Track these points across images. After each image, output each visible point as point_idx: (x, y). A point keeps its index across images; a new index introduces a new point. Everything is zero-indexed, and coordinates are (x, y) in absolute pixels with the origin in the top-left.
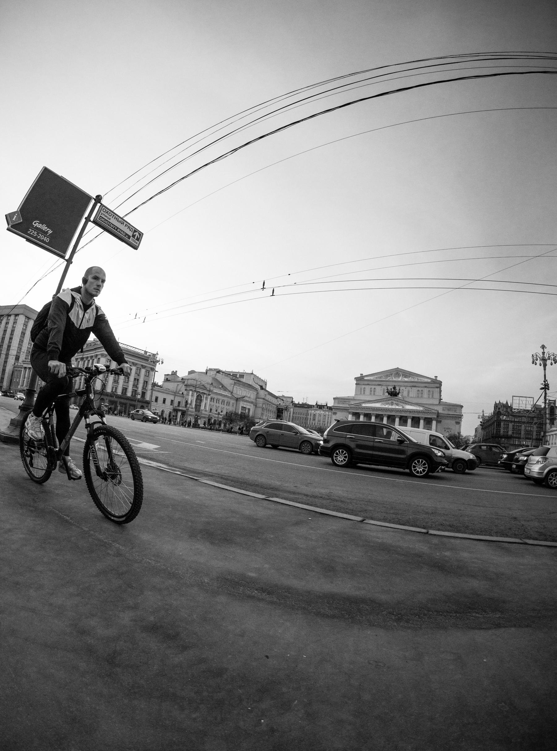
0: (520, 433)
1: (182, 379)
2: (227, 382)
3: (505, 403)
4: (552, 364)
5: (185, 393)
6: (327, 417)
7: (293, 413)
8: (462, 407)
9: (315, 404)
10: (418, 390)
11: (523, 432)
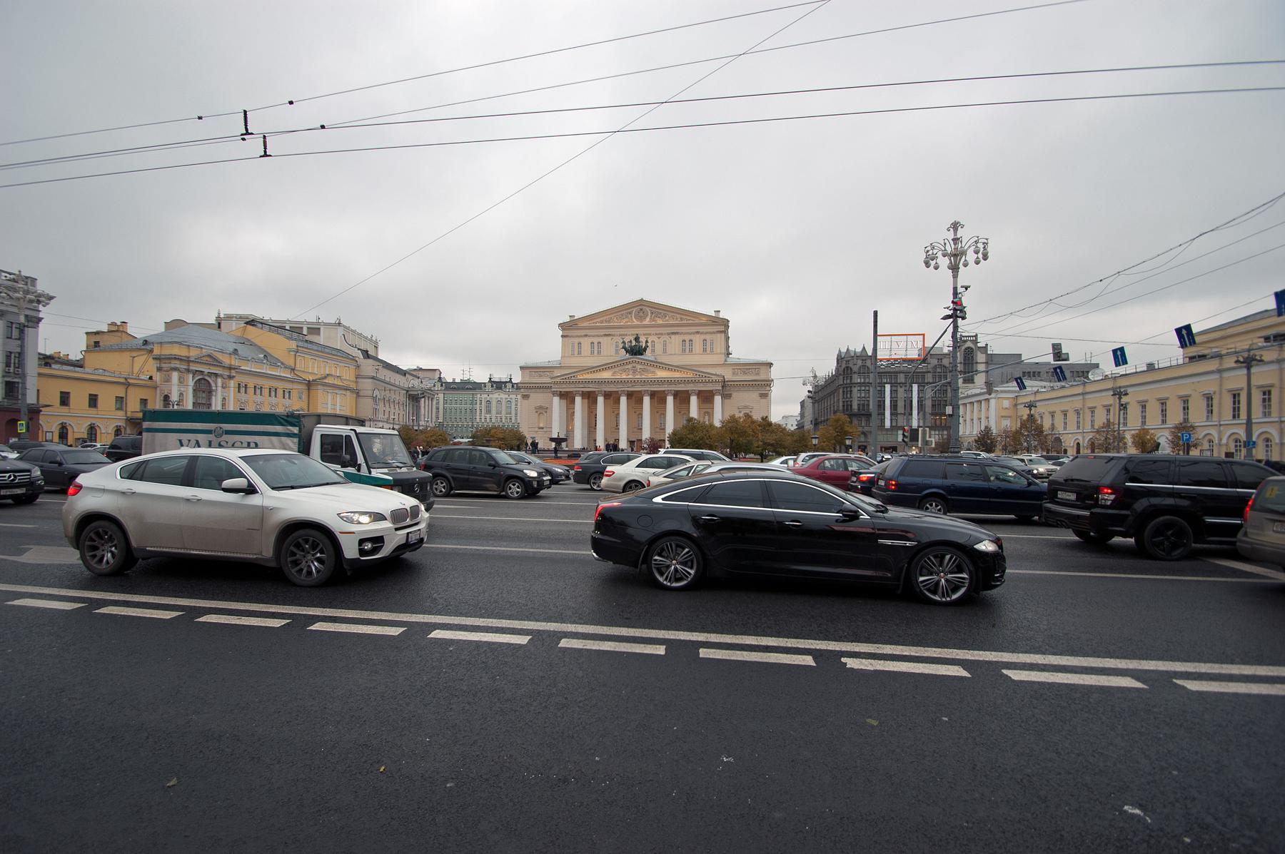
1: (146, 342)
2: (280, 346)
3: (859, 350)
4: (977, 263)
5: (158, 377)
7: (445, 402)
8: (770, 365)
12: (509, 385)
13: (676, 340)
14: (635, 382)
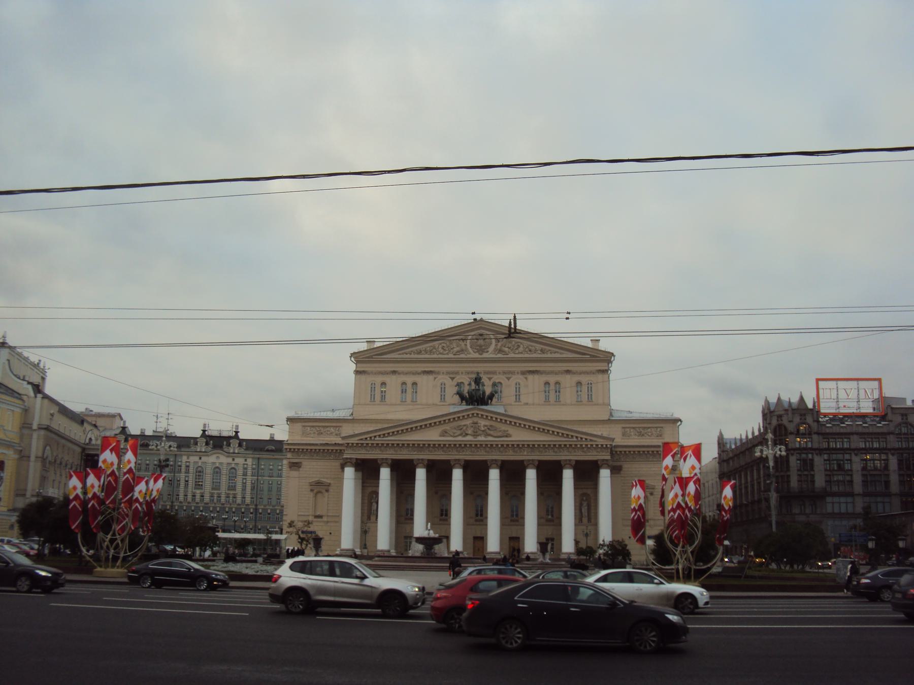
0: (851, 482)
3: (795, 400)
6: (240, 472)
8: (676, 421)
9: (198, 434)
10: (404, 383)
12: (234, 443)
13: (535, 382)
14: (477, 447)
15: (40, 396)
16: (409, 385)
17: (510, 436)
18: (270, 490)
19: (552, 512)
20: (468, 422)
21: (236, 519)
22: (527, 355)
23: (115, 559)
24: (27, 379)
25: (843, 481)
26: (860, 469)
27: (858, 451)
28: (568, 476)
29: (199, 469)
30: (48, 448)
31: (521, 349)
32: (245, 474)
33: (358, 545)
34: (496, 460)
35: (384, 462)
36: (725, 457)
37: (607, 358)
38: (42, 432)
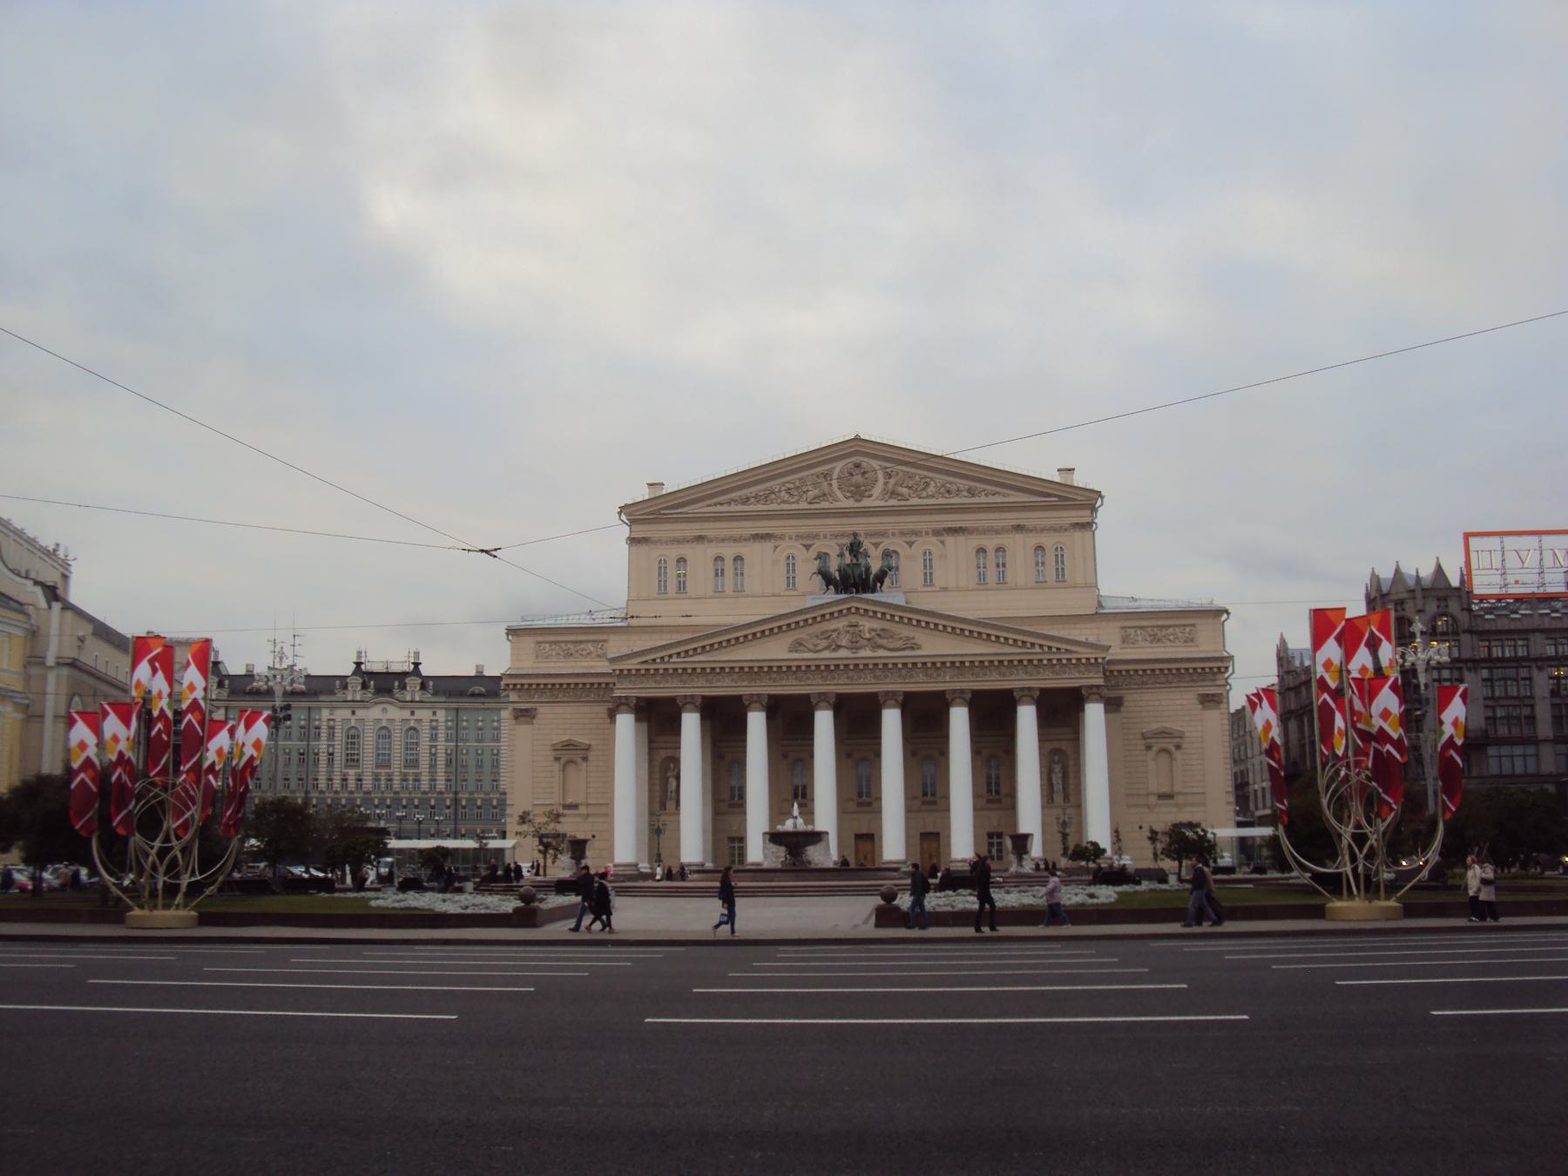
0: (1531, 719)
3: (1427, 572)
8: (1218, 613)
9: (348, 670)
10: (719, 559)
11: (1543, 712)
12: (413, 683)
13: (959, 548)
14: (858, 668)
15: (57, 606)
16: (729, 563)
17: (919, 648)
18: (480, 765)
19: (998, 784)
20: (841, 624)
21: (421, 817)
22: (942, 501)
23: (171, 890)
24: (33, 575)
25: (1518, 718)
26: (1547, 693)
27: (1544, 662)
28: (1027, 717)
29: (352, 732)
30: (77, 699)
31: (931, 489)
32: (434, 738)
33: (645, 854)
34: (894, 693)
35: (688, 702)
36: (1291, 681)
37: (1089, 500)
38: (65, 671)
